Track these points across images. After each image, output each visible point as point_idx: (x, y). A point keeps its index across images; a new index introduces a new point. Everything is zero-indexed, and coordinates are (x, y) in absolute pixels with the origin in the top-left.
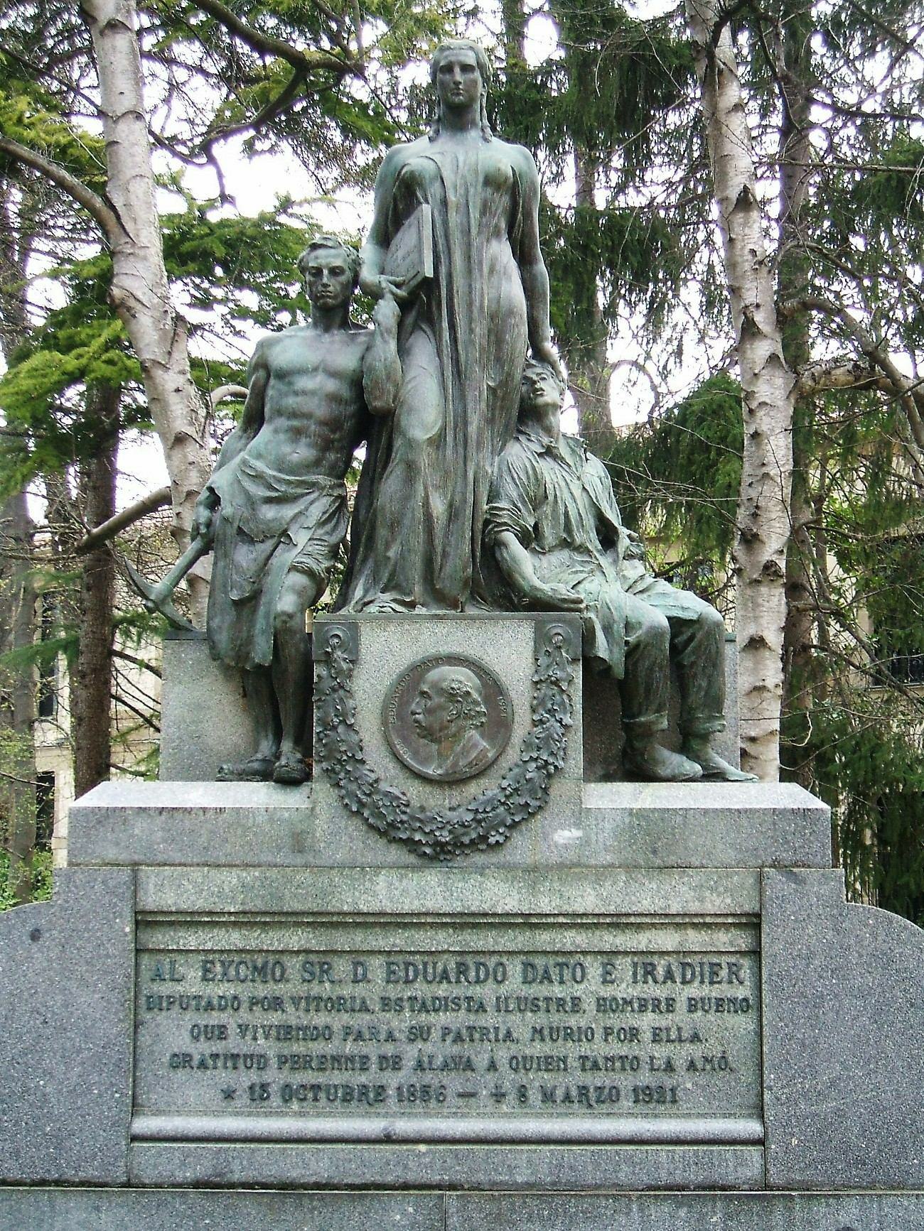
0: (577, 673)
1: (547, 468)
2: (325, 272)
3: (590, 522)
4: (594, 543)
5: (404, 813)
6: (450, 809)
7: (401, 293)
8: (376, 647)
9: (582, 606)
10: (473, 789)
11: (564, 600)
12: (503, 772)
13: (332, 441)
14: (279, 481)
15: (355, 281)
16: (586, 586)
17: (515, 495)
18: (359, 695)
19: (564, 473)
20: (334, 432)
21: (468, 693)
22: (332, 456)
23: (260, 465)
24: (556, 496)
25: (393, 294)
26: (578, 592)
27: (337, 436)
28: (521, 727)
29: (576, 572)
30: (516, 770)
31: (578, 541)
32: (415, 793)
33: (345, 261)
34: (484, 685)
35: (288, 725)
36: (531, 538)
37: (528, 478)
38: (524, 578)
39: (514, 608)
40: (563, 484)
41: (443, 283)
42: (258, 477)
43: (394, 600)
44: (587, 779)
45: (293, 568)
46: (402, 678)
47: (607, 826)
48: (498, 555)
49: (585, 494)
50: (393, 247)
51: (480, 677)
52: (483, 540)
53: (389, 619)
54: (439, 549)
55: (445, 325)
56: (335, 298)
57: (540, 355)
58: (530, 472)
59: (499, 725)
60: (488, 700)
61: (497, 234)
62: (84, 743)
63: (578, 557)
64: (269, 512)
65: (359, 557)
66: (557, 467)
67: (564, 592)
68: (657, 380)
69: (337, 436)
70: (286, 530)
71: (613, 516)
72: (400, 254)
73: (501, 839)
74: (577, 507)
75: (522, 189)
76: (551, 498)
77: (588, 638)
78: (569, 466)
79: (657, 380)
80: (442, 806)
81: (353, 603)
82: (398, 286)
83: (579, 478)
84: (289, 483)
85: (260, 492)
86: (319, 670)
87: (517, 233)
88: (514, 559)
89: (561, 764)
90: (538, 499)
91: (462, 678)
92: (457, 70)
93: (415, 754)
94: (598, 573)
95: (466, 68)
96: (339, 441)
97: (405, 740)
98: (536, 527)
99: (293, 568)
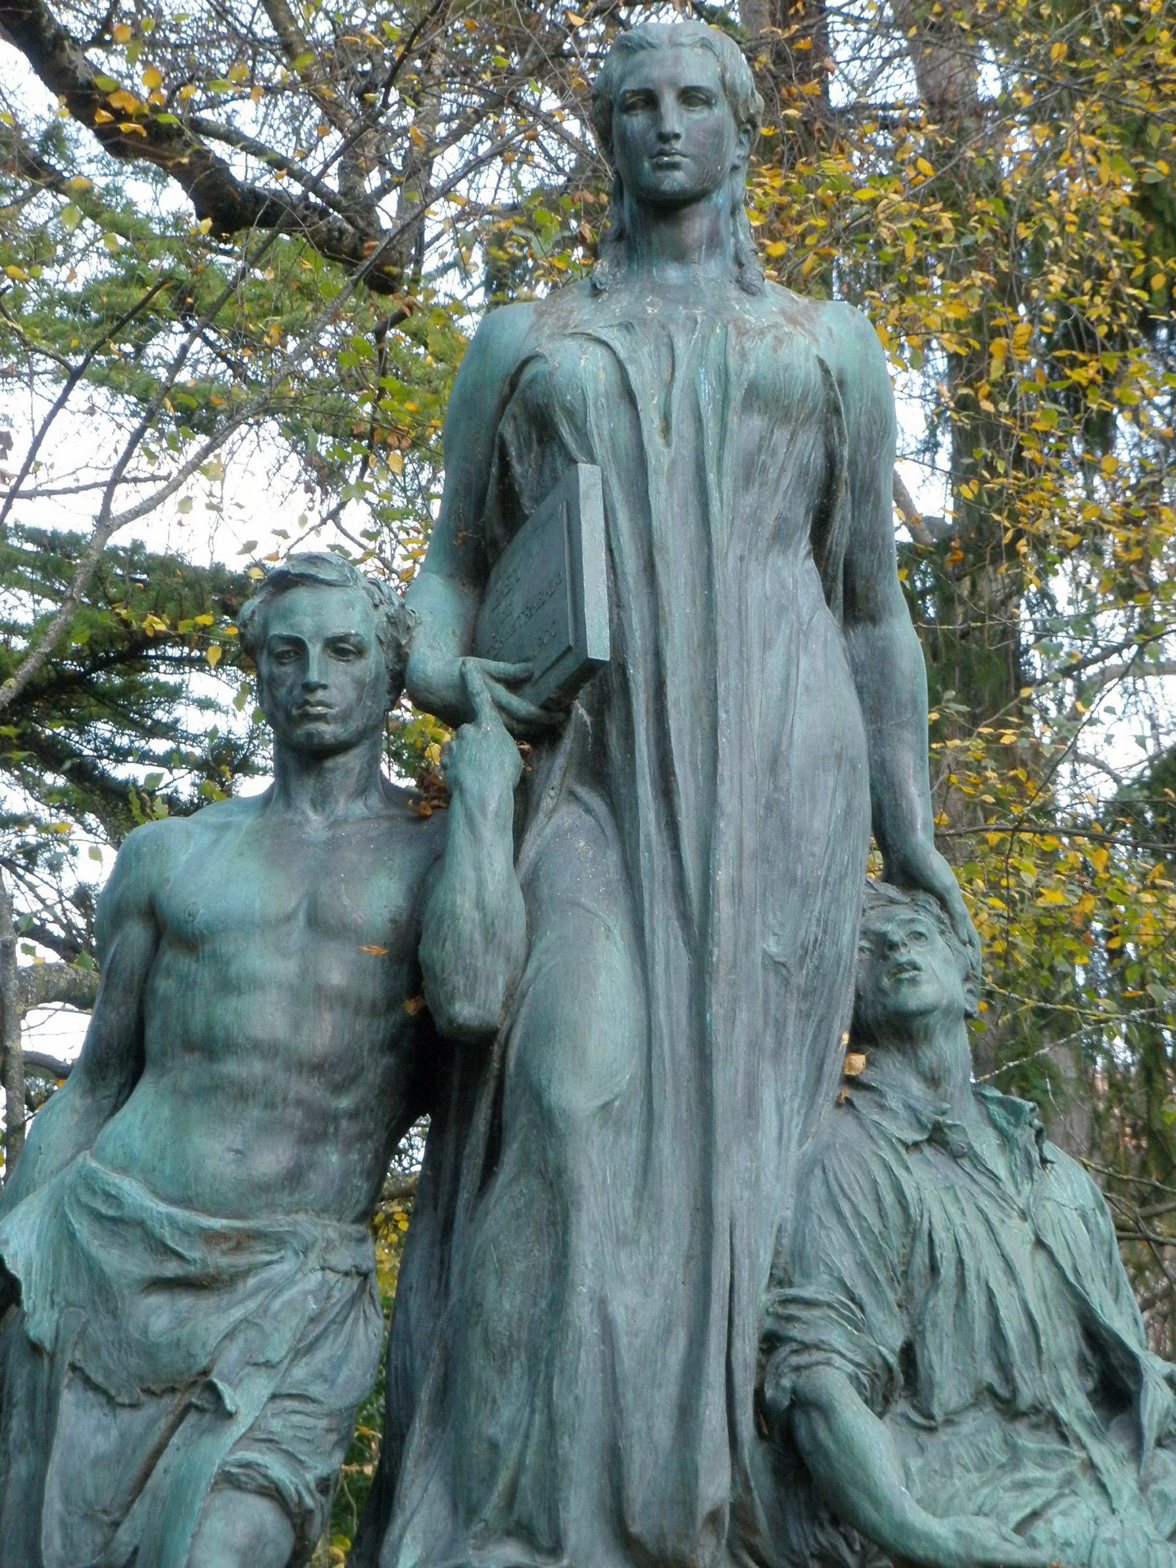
1: (926, 1181)
2: (315, 650)
3: (1062, 1339)
4: (1074, 1402)
7: (522, 705)
13: (335, 1118)
14: (186, 1232)
15: (399, 680)
16: (1058, 1524)
17: (846, 1265)
19: (984, 1202)
20: (338, 1089)
22: (332, 1158)
23: (134, 1192)
24: (961, 1262)
25: (501, 707)
26: (1033, 1543)
27: (345, 1102)
29: (1025, 1485)
31: (1026, 1396)
33: (366, 618)
36: (900, 1382)
37: (882, 1214)
38: (876, 1502)
40: (980, 1230)
41: (639, 676)
42: (120, 1223)
45: (228, 1480)
48: (802, 1434)
49: (1041, 1259)
50: (497, 582)
52: (759, 1393)
54: (976, 1176)
55: (646, 790)
56: (344, 718)
57: (905, 874)
58: (889, 1198)
61: (781, 536)
63: (1028, 1440)
64: (158, 1315)
65: (464, 1196)
66: (961, 1181)
67: (992, 1540)
69: (345, 1102)
70: (205, 1372)
71: (1124, 1320)
72: (517, 601)
74: (1025, 1296)
75: (853, 416)
76: (947, 1271)
78: (995, 1178)
82: (514, 684)
83: (1024, 1216)
84: (211, 1237)
85: (122, 1262)
87: (839, 535)
88: (846, 1445)
90: (916, 1266)
92: (669, 101)
94: (1085, 1485)
95: (690, 96)
96: (354, 1115)
98: (908, 1354)
99: (228, 1480)
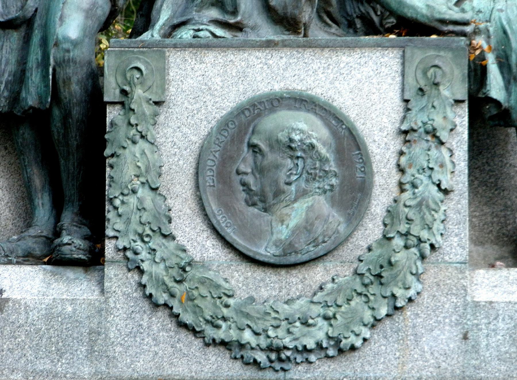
0: (461, 118)
5: (227, 306)
6: (286, 303)
8: (190, 83)
9: (468, 29)
10: (318, 274)
11: (443, 22)
12: (359, 253)
18: (166, 149)
21: (312, 147)
26: (463, 11)
28: (382, 196)
30: (377, 252)
32: (240, 279)
34: (334, 133)
35: (70, 190)
39: (371, 29)
43: (217, 22)
44: (473, 263)
46: (224, 125)
47: (501, 325)
51: (328, 125)
53: (208, 46)
59: (353, 194)
60: (340, 153)
62: (296, 91)
68: (379, 202)
73: (358, 343)
77: (478, 74)
79: (379, 202)
80: (277, 299)
81: (157, 27)
86: (113, 114)
89: (437, 240)
91: (305, 126)
93: (242, 228)
97: (228, 207)
